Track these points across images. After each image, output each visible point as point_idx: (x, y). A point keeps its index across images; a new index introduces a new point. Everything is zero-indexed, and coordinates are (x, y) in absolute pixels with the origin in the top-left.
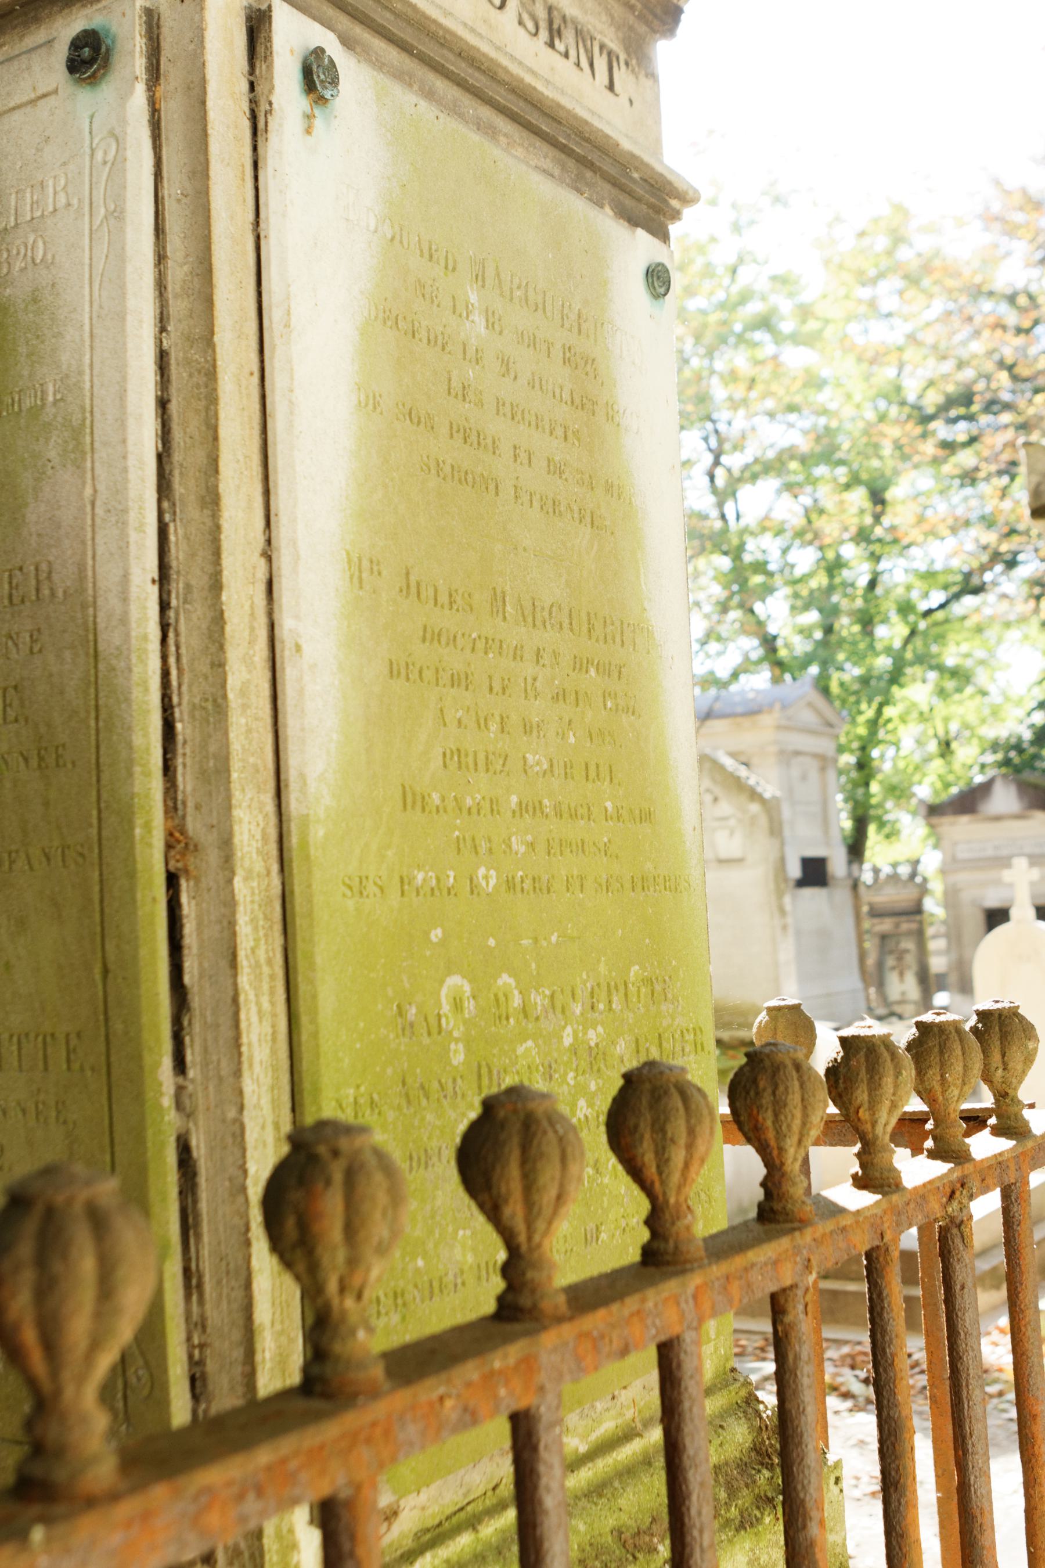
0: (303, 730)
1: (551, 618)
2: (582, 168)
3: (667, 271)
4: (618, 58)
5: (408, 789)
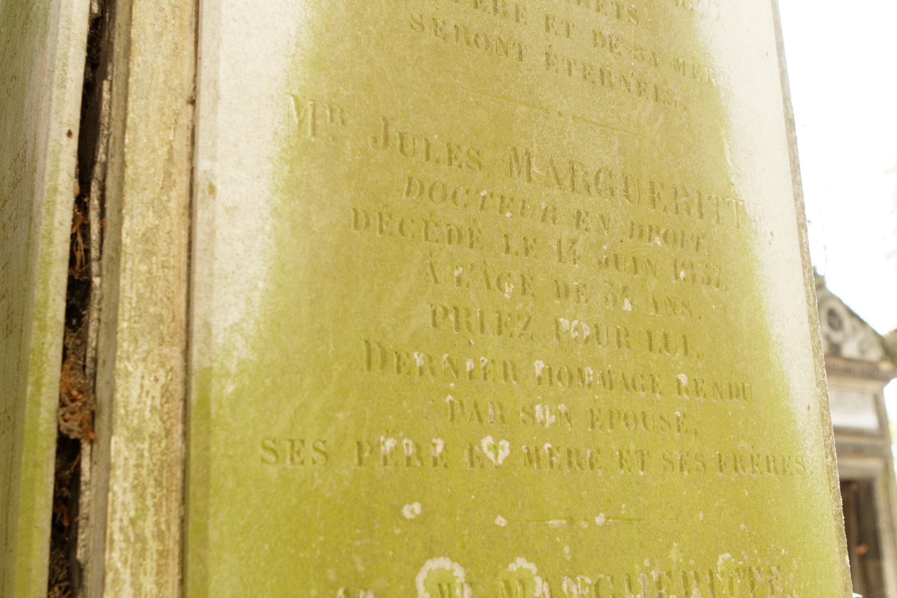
0: (211, 275)
5: (374, 345)
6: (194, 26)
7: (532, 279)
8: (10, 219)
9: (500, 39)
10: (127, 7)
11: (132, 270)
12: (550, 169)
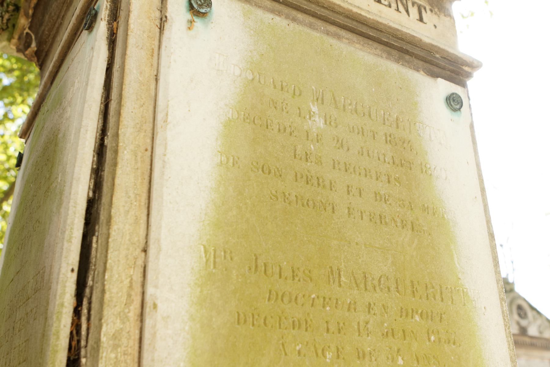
0: (153, 360)
1: (379, 285)
2: (402, 54)
3: (460, 97)
4: (425, 9)
6: (147, 205)
7: (343, 349)
8: (31, 311)
9: (321, 201)
10: (109, 195)
11: (106, 357)
12: (352, 278)
